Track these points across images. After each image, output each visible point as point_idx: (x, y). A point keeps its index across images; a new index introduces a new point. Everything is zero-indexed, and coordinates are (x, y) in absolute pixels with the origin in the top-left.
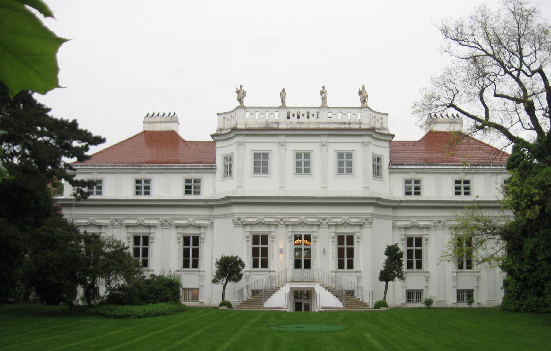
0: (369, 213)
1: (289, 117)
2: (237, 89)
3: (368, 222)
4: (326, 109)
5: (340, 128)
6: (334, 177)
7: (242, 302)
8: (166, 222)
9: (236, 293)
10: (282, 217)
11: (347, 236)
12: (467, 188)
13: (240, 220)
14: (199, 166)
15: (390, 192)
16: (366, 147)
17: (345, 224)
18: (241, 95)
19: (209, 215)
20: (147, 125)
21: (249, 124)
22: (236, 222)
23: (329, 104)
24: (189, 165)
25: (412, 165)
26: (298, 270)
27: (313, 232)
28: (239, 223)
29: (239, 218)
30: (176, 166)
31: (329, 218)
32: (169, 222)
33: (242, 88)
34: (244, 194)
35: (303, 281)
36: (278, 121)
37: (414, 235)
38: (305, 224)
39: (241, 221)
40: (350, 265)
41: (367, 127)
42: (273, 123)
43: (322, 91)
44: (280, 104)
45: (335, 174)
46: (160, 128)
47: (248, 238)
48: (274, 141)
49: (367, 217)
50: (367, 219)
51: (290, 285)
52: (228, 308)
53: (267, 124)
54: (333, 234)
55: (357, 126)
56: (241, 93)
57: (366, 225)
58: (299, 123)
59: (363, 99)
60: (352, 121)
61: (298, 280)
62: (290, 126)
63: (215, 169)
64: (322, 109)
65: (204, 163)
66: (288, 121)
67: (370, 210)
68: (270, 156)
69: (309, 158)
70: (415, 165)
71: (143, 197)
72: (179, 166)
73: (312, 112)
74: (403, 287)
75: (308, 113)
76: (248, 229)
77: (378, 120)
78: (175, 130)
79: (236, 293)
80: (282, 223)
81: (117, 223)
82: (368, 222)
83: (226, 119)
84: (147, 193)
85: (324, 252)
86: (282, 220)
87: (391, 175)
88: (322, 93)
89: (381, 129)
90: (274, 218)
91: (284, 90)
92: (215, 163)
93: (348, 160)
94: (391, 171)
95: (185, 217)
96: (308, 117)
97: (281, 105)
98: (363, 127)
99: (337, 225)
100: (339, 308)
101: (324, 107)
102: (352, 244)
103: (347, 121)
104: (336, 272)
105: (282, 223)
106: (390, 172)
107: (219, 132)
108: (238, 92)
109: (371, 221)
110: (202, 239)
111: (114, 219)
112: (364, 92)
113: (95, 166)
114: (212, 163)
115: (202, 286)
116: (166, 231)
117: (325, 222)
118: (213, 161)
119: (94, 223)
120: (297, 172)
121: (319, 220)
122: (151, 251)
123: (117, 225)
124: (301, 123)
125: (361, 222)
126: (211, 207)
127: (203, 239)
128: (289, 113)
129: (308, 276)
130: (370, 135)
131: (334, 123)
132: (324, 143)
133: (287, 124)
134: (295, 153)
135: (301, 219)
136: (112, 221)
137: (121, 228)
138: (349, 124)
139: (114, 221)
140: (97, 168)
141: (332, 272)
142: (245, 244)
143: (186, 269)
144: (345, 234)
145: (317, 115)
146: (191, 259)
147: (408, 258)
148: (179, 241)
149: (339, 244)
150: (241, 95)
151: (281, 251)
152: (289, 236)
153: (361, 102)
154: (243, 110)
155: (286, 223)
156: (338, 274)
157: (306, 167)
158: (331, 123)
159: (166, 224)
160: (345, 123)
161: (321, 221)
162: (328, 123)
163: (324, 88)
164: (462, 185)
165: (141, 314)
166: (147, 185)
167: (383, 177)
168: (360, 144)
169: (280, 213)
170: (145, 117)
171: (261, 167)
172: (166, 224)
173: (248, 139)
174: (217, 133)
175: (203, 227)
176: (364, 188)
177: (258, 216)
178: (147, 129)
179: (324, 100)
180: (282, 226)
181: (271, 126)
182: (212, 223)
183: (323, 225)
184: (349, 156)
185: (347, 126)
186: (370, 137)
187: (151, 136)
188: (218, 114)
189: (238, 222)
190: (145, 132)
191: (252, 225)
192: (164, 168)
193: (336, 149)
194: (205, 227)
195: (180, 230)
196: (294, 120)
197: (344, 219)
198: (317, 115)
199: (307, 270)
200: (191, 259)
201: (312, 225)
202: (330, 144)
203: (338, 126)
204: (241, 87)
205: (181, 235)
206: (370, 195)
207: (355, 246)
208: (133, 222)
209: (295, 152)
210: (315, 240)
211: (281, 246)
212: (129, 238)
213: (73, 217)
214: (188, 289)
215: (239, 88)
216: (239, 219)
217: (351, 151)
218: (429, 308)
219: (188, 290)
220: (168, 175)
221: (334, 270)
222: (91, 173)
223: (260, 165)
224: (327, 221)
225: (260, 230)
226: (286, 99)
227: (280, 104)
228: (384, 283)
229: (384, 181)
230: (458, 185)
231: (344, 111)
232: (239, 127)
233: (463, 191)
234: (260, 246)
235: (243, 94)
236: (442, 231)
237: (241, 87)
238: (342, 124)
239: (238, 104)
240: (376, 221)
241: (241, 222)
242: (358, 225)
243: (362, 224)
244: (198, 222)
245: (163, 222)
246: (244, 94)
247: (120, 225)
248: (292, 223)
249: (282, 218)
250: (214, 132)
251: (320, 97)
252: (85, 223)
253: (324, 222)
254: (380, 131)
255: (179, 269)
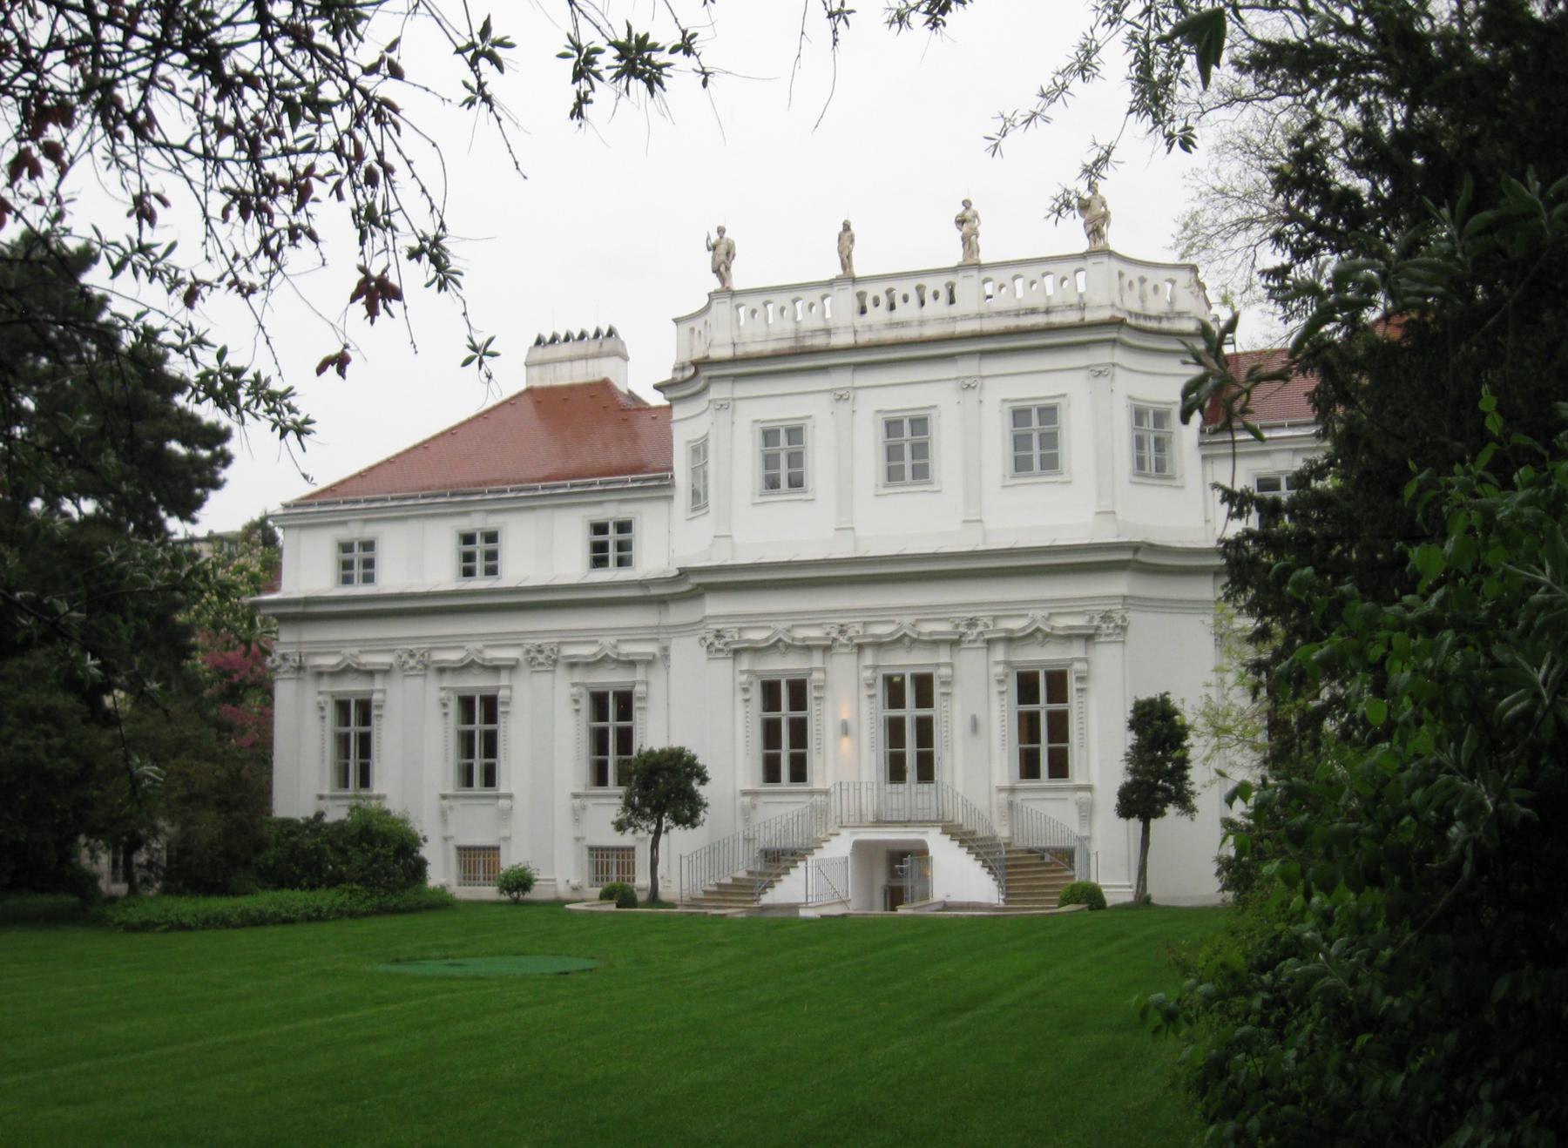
0: (1116, 597)
1: (863, 311)
2: (708, 239)
3: (1112, 625)
4: (975, 273)
5: (1017, 327)
6: (1004, 487)
7: (715, 889)
8: (540, 652)
9: (685, 862)
10: (843, 621)
11: (788, 682)
12: (623, 546)
13: (723, 637)
14: (627, 482)
15: (1207, 521)
16: (1102, 383)
17: (1034, 636)
18: (722, 256)
19: (657, 627)
20: (536, 371)
21: (744, 343)
22: (712, 644)
23: (985, 257)
24: (597, 480)
25: (1282, 427)
26: (900, 787)
27: (938, 665)
28: (721, 647)
29: (718, 631)
30: (564, 486)
31: (985, 620)
32: (547, 652)
33: (726, 235)
34: (1118, 536)
35: (909, 821)
36: (831, 325)
37: (1040, 663)
38: (1047, 635)
39: (727, 640)
40: (1059, 767)
41: (1105, 315)
42: (814, 332)
43: (962, 215)
44: (836, 270)
45: (1004, 476)
46: (571, 377)
47: (745, 690)
48: (1002, 372)
49: (1108, 608)
50: (1106, 617)
51: (852, 833)
52: (618, 906)
53: (797, 338)
54: (1000, 669)
55: (1072, 317)
56: (722, 249)
57: (1107, 635)
58: (892, 325)
59: (1090, 227)
60: (1055, 301)
61: (927, 818)
62: (863, 338)
63: (671, 486)
64: (961, 274)
65: (654, 471)
66: (860, 321)
67: (1119, 585)
68: (1062, 415)
69: (925, 431)
70: (1292, 426)
71: (480, 582)
72: (573, 486)
73: (932, 284)
74: (578, 839)
75: (920, 289)
76: (745, 663)
77: (1131, 284)
78: (613, 380)
79: (685, 862)
80: (843, 640)
81: (412, 662)
82: (1112, 625)
83: (696, 332)
84: (491, 571)
85: (975, 726)
86: (842, 632)
87: (1208, 467)
88: (961, 221)
89: (1169, 318)
90: (820, 625)
91: (847, 227)
92: (670, 469)
93: (1047, 428)
94: (1207, 452)
95: (588, 637)
96: (892, 307)
97: (840, 272)
98: (1090, 316)
99: (1010, 640)
100: (990, 907)
101: (970, 264)
102: (1064, 699)
103: (1040, 303)
104: (1012, 790)
105: (843, 640)
106: (1204, 458)
107: (679, 376)
108: (713, 248)
109: (1119, 622)
110: (815, 687)
111: (405, 651)
112: (1095, 203)
113: (358, 502)
114: (661, 470)
115: (507, 839)
116: (543, 680)
117: (975, 631)
118: (663, 465)
119: (479, 661)
120: (1016, 470)
121: (957, 626)
122: (815, 737)
123: (412, 668)
124: (897, 323)
125: (955, 633)
126: (662, 602)
127: (643, 699)
128: (861, 296)
129: (926, 806)
130: (1114, 342)
131: (999, 313)
132: (968, 382)
133: (855, 332)
134: (758, 428)
135: (901, 626)
136: (400, 657)
137: (425, 676)
138: (1048, 311)
139: (405, 657)
140: (358, 507)
141: (1000, 790)
142: (740, 709)
143: (600, 790)
144: (1041, 667)
145: (951, 293)
146: (1044, 747)
147: (919, 746)
148: (747, 697)
149: (1021, 701)
150: (722, 256)
151: (845, 730)
152: (866, 679)
153: (1088, 236)
154: (728, 300)
155: (856, 641)
156: (1018, 798)
157: (916, 462)
158: (990, 315)
159: (544, 660)
160: (1033, 311)
161: (962, 629)
162: (980, 316)
163: (967, 204)
164: (358, 555)
165: (235, 919)
166: (368, 555)
167: (1178, 475)
168: (1083, 374)
169: (836, 611)
170: (530, 349)
171: (1036, 452)
172: (541, 658)
173: (863, 379)
174: (673, 379)
175: (641, 662)
176: (1097, 513)
177: (772, 624)
178: (537, 384)
179: (968, 242)
180: (721, 655)
181: (808, 342)
182: (665, 649)
183: (970, 641)
184: (1049, 413)
185: (1040, 320)
186: (1113, 347)
187: (565, 400)
188: (677, 321)
189: (716, 642)
190: (530, 391)
191: (756, 650)
192: (530, 494)
193: (757, 418)
194: (649, 663)
195: (449, 681)
196: (878, 315)
197: (1034, 621)
198: (951, 293)
199: (926, 787)
200: (1044, 747)
201: (935, 643)
202: (988, 382)
203: (1012, 323)
204: (721, 231)
205: (329, 699)
206: (1118, 536)
207: (1074, 705)
208: (454, 656)
209: (880, 416)
210: (944, 690)
211: (846, 713)
212: (322, 709)
213: (305, 650)
214: (608, 849)
215: (715, 237)
216: (719, 635)
217: (1055, 397)
218: (517, 902)
219: (620, 853)
220: (545, 515)
221: (1006, 783)
222: (345, 523)
223: (1030, 448)
224: (980, 628)
225: (782, 666)
226: (853, 253)
227: (836, 270)
228: (1135, 824)
229: (1182, 487)
230: (468, 548)
231: (1033, 272)
232: (715, 354)
233: (612, 554)
234: (1043, 707)
235: (728, 254)
236: (419, 681)
237: (721, 231)
238: (1026, 314)
239: (716, 284)
240: (1139, 621)
241: (726, 644)
242: (1079, 636)
243: (1092, 632)
244: (626, 649)
245: (532, 655)
246: (730, 254)
247: (420, 667)
248: (1003, 635)
249: (842, 626)
250: (666, 375)
251: (957, 235)
252: (332, 666)
253: (973, 633)
254: (1165, 325)
255: (450, 791)
